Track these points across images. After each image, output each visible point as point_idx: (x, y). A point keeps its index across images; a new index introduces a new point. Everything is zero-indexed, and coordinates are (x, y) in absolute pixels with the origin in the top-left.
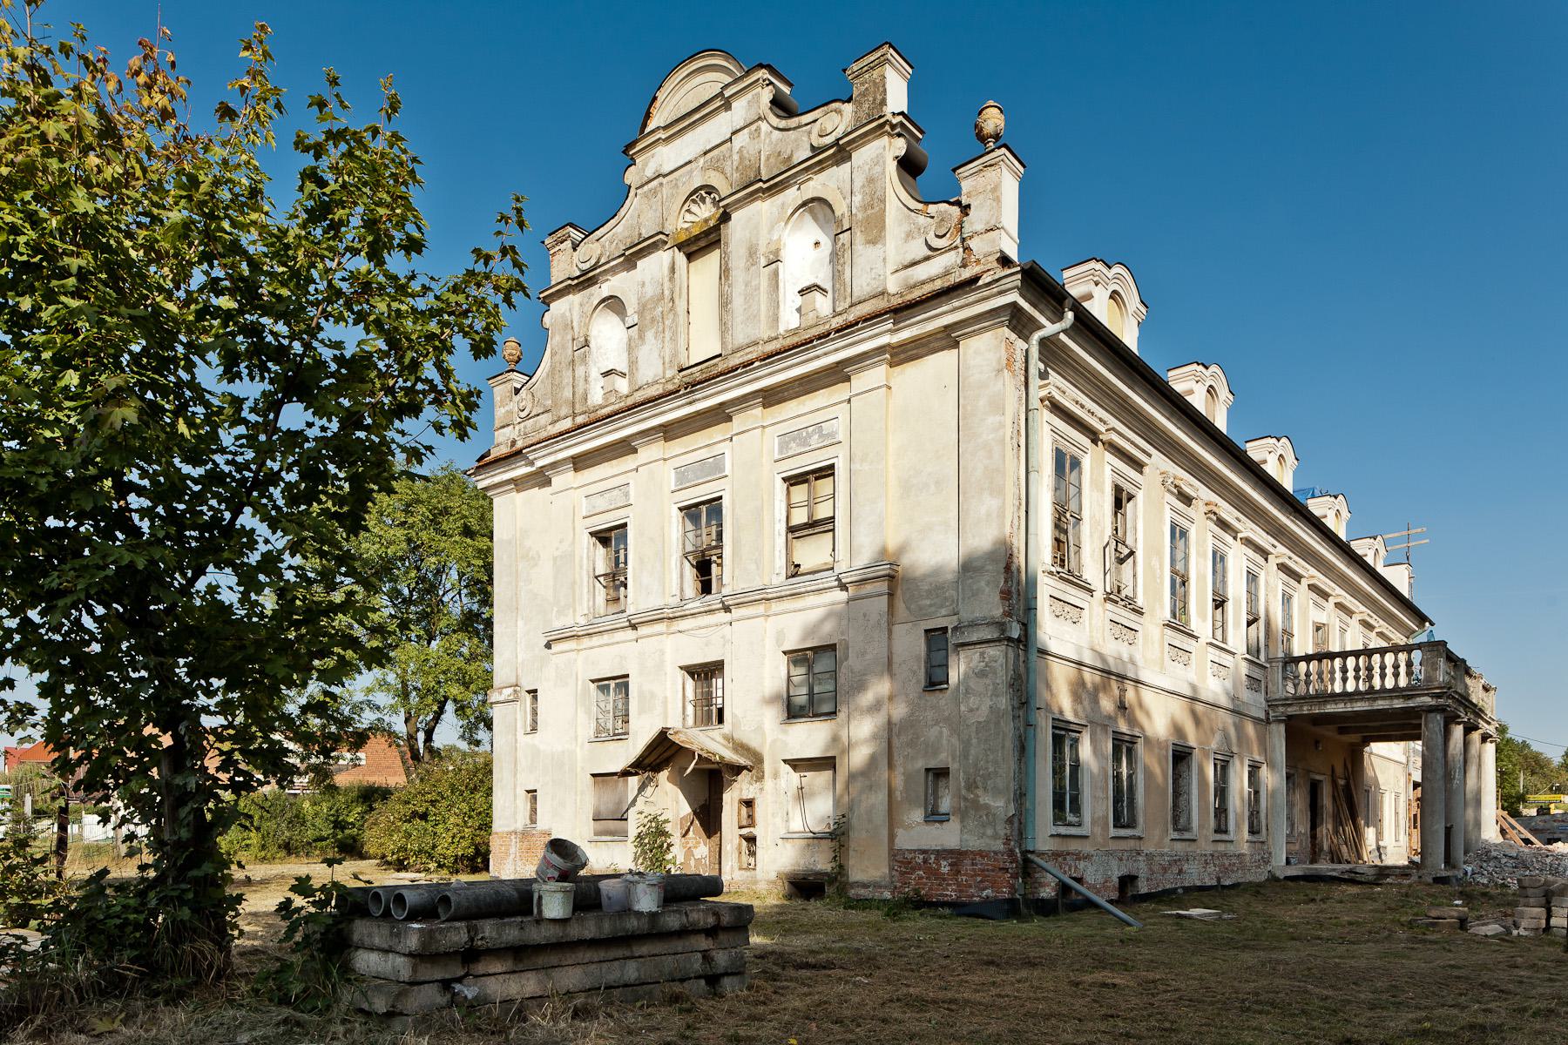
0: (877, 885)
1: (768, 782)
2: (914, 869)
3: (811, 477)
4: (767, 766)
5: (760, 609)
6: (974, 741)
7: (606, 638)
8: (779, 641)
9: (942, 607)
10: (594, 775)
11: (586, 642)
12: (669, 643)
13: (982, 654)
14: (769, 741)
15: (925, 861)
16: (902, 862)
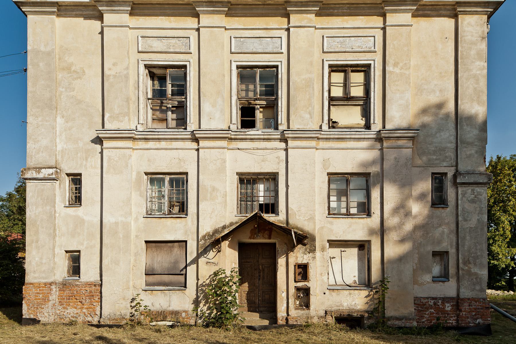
0: (407, 318)
1: (318, 254)
2: (427, 309)
3: (350, 69)
4: (318, 244)
5: (224, 143)
6: (468, 238)
7: (163, 144)
8: (325, 166)
9: (444, 161)
10: (146, 242)
11: (142, 144)
12: (229, 155)
13: (473, 190)
14: (317, 227)
15: (435, 304)
16: (421, 304)
